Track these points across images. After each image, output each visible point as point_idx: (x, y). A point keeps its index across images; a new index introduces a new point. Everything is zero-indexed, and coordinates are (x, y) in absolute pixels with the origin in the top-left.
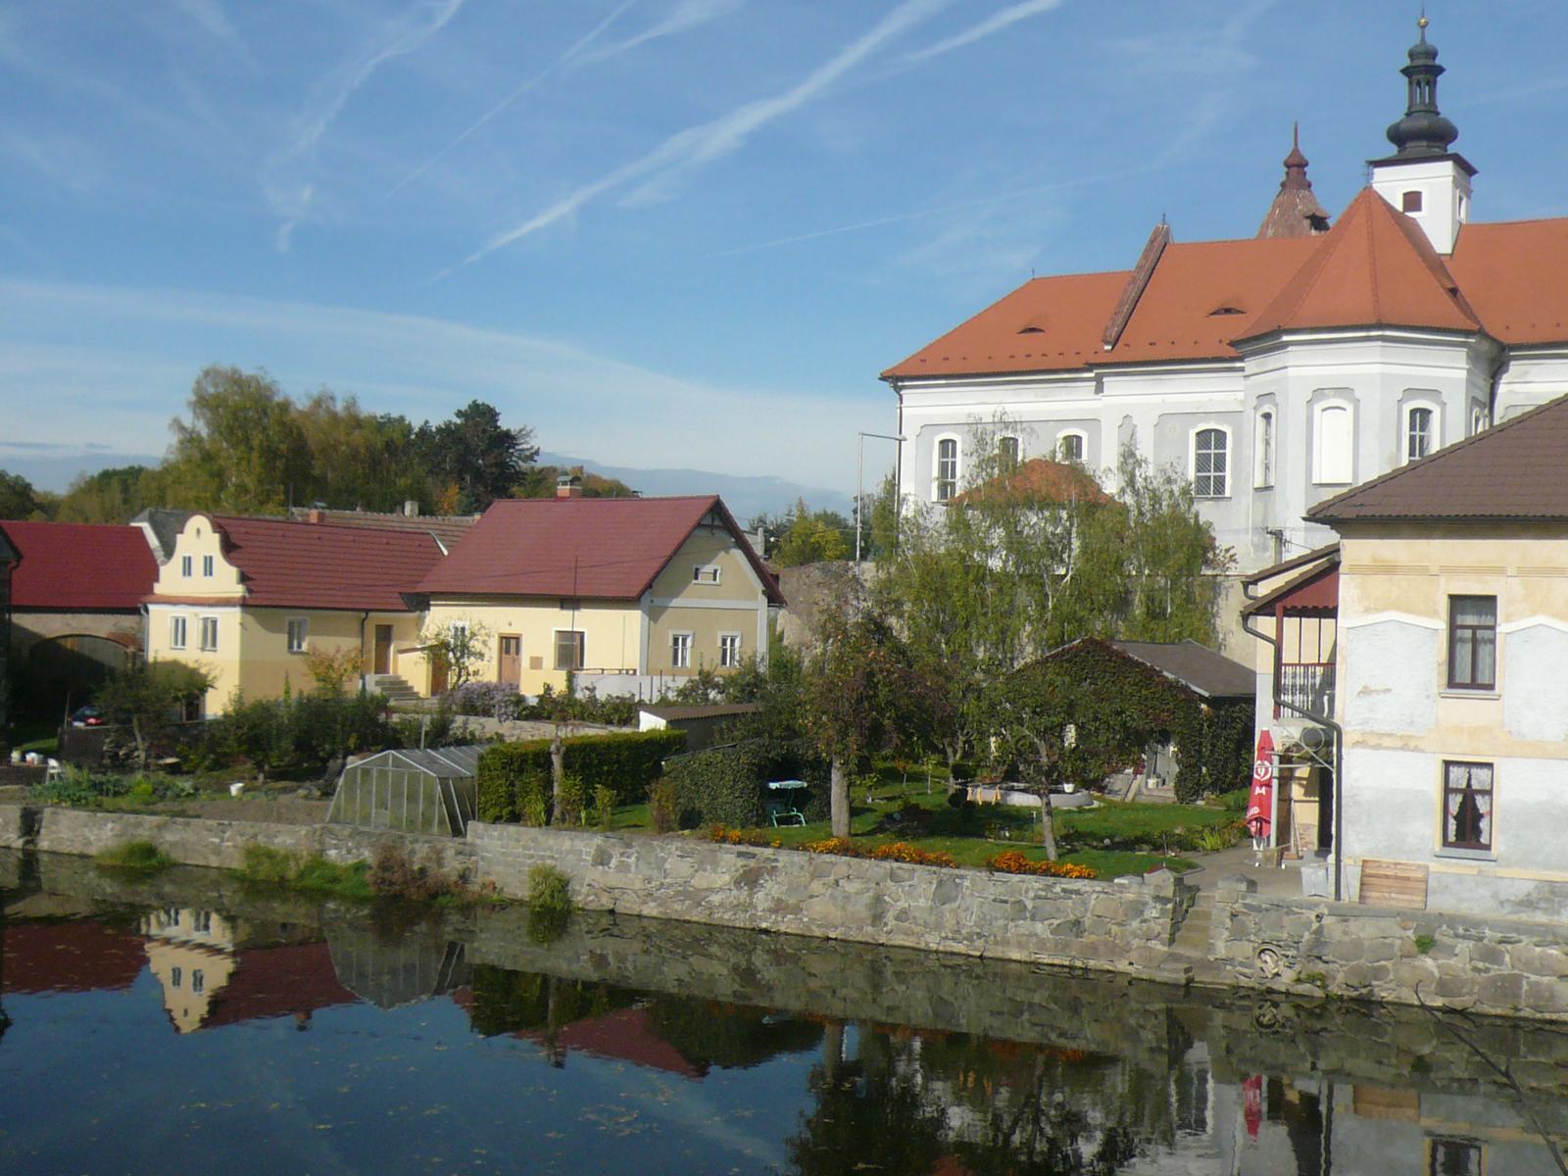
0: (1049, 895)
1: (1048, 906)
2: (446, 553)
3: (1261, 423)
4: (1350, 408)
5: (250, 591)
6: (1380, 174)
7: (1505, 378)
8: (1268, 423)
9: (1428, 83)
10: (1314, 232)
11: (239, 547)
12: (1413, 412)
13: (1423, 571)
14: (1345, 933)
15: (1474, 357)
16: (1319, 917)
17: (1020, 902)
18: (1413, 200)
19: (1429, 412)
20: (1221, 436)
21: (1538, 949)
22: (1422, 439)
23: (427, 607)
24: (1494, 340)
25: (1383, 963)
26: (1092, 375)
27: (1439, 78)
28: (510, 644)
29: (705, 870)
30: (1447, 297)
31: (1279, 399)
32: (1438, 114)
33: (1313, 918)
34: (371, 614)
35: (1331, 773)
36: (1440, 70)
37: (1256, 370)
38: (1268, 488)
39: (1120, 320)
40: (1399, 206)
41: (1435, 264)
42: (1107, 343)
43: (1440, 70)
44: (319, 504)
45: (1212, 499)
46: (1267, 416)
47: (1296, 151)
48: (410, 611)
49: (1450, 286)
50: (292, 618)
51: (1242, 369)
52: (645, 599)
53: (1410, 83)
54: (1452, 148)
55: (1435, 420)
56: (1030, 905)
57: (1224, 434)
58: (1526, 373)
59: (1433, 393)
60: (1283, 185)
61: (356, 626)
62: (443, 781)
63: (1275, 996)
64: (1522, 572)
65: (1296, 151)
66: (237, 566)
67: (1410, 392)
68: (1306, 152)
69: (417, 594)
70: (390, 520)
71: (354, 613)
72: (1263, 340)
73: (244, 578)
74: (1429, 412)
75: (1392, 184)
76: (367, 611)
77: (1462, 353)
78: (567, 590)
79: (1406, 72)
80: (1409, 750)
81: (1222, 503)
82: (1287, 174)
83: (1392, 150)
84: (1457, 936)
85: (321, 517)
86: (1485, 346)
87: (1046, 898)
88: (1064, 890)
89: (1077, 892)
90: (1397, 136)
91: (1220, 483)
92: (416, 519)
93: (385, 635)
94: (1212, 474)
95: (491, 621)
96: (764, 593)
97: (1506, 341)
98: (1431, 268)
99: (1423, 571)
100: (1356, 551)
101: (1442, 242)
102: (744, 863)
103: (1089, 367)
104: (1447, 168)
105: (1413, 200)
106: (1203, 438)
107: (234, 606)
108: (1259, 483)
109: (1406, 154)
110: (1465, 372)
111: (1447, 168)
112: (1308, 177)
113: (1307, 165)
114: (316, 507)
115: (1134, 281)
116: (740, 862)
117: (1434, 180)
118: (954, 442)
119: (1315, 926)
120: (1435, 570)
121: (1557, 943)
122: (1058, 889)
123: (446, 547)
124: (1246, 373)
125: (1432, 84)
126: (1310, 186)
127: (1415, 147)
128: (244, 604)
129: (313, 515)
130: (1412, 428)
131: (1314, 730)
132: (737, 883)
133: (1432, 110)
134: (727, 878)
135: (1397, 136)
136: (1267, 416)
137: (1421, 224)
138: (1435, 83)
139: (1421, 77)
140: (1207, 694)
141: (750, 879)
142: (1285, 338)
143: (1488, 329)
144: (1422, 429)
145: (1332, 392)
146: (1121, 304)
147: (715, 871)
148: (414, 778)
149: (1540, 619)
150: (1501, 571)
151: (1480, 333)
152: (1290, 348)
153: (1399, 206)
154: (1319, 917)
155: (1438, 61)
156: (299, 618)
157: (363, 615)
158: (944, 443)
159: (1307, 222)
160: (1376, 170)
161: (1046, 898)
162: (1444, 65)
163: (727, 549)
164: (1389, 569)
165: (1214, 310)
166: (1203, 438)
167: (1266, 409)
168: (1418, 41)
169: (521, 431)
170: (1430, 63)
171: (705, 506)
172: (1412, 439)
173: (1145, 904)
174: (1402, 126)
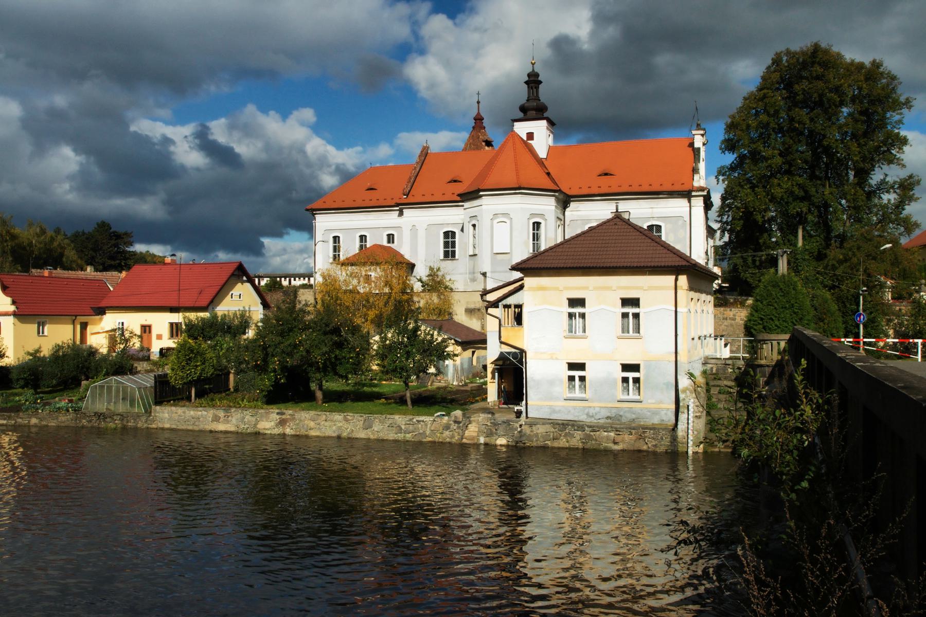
0: (411, 423)
1: (411, 428)
2: (112, 289)
3: (472, 228)
4: (508, 221)
5: (17, 308)
6: (517, 124)
7: (567, 209)
8: (475, 229)
9: (536, 88)
10: (487, 148)
11: (8, 287)
12: (534, 223)
13: (557, 289)
14: (532, 431)
15: (558, 200)
16: (521, 426)
17: (399, 426)
18: (530, 136)
19: (540, 223)
20: (453, 233)
21: (606, 433)
22: (537, 234)
23: (104, 313)
24: (565, 193)
25: (546, 442)
26: (398, 208)
27: (540, 86)
28: (146, 329)
29: (263, 421)
30: (546, 176)
31: (479, 218)
32: (540, 100)
33: (518, 426)
34: (78, 317)
35: (522, 369)
36: (541, 82)
37: (469, 207)
38: (475, 255)
39: (410, 185)
40: (525, 138)
41: (540, 162)
42: (405, 195)
43: (541, 82)
44: (49, 268)
45: (451, 260)
46: (474, 226)
47: (479, 113)
48: (96, 315)
49: (547, 171)
50: (39, 320)
51: (463, 206)
52: (210, 307)
53: (528, 87)
54: (545, 115)
55: (542, 226)
56: (403, 427)
57: (455, 233)
58: (578, 207)
59: (542, 215)
60: (474, 128)
61: (71, 322)
62: (139, 389)
63: (270, 550)
64: (596, 288)
65: (479, 113)
66: (11, 297)
67: (533, 215)
68: (483, 114)
69: (99, 308)
70: (80, 274)
71: (70, 317)
72: (472, 195)
73: (14, 303)
74: (540, 223)
75: (520, 129)
76: (76, 316)
77: (554, 198)
78: (174, 304)
79: (526, 83)
80: (553, 359)
81: (454, 261)
82: (475, 123)
83: (521, 115)
84: (575, 430)
85: (50, 273)
86: (561, 197)
87: (410, 424)
88: (417, 421)
89: (423, 421)
90: (523, 109)
91: (454, 253)
92: (93, 273)
93: (84, 326)
94: (450, 249)
95: (133, 321)
96: (261, 303)
97: (569, 193)
98: (539, 164)
99: (557, 289)
100: (529, 281)
101: (542, 154)
102: (280, 417)
103: (397, 205)
104: (544, 123)
105: (530, 136)
106: (446, 234)
107: (10, 315)
108: (471, 253)
109: (526, 117)
110: (554, 207)
111: (544, 123)
112: (484, 124)
113: (483, 119)
114: (47, 269)
115: (415, 168)
116: (278, 417)
117: (539, 128)
118: (339, 237)
119: (519, 429)
120: (561, 288)
121: (613, 431)
122: (415, 420)
123: (112, 286)
124: (465, 207)
125: (537, 88)
126: (485, 128)
127: (532, 113)
128: (15, 314)
129: (46, 273)
130: (534, 230)
131: (515, 353)
132: (277, 425)
133: (537, 99)
134: (273, 423)
135: (523, 109)
136: (474, 226)
137: (534, 146)
138: (538, 87)
139: (533, 85)
140: (460, 341)
141: (282, 423)
142: (481, 193)
143: (562, 189)
144: (537, 230)
145: (501, 215)
146: (410, 178)
147: (267, 421)
148: (125, 389)
149: (603, 306)
150: (586, 288)
151: (560, 191)
152: (483, 197)
153: (525, 138)
154: (521, 426)
155: (540, 79)
156: (43, 320)
157: (74, 318)
158: (335, 238)
159: (484, 144)
160: (515, 123)
161: (410, 424)
162: (542, 80)
163: (243, 282)
164: (542, 288)
165: (449, 181)
166: (446, 234)
167: (473, 222)
168: (531, 70)
169: (126, 234)
170: (536, 79)
171: (236, 266)
172: (534, 234)
173: (450, 424)
174: (526, 105)
